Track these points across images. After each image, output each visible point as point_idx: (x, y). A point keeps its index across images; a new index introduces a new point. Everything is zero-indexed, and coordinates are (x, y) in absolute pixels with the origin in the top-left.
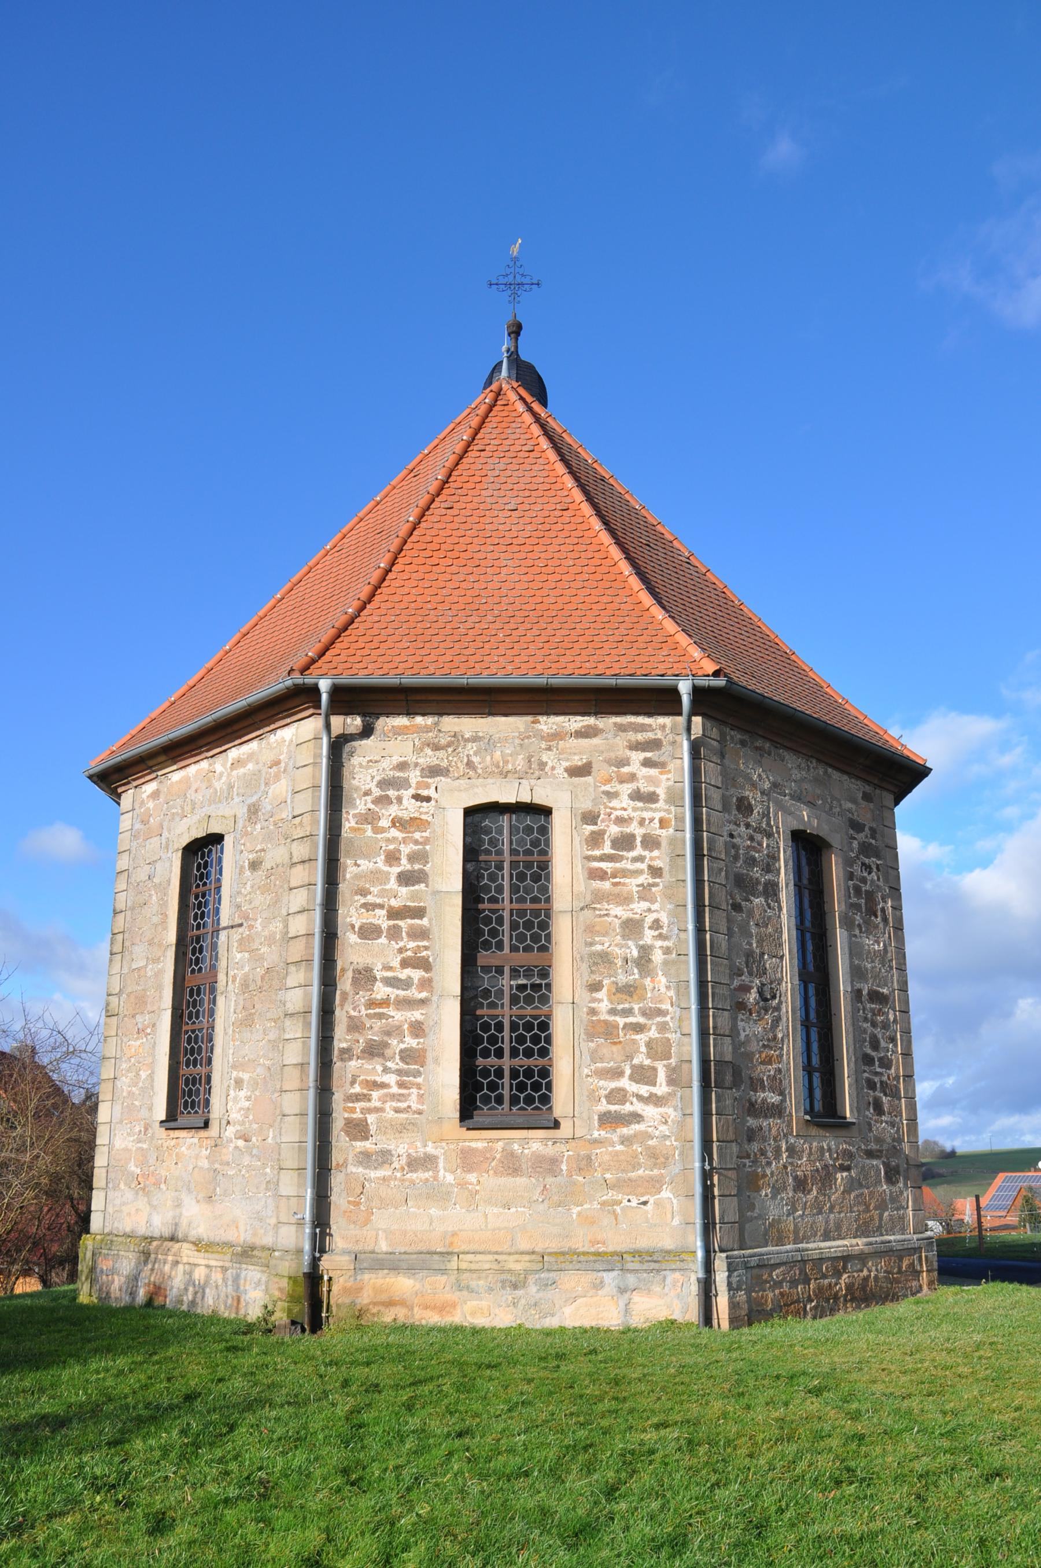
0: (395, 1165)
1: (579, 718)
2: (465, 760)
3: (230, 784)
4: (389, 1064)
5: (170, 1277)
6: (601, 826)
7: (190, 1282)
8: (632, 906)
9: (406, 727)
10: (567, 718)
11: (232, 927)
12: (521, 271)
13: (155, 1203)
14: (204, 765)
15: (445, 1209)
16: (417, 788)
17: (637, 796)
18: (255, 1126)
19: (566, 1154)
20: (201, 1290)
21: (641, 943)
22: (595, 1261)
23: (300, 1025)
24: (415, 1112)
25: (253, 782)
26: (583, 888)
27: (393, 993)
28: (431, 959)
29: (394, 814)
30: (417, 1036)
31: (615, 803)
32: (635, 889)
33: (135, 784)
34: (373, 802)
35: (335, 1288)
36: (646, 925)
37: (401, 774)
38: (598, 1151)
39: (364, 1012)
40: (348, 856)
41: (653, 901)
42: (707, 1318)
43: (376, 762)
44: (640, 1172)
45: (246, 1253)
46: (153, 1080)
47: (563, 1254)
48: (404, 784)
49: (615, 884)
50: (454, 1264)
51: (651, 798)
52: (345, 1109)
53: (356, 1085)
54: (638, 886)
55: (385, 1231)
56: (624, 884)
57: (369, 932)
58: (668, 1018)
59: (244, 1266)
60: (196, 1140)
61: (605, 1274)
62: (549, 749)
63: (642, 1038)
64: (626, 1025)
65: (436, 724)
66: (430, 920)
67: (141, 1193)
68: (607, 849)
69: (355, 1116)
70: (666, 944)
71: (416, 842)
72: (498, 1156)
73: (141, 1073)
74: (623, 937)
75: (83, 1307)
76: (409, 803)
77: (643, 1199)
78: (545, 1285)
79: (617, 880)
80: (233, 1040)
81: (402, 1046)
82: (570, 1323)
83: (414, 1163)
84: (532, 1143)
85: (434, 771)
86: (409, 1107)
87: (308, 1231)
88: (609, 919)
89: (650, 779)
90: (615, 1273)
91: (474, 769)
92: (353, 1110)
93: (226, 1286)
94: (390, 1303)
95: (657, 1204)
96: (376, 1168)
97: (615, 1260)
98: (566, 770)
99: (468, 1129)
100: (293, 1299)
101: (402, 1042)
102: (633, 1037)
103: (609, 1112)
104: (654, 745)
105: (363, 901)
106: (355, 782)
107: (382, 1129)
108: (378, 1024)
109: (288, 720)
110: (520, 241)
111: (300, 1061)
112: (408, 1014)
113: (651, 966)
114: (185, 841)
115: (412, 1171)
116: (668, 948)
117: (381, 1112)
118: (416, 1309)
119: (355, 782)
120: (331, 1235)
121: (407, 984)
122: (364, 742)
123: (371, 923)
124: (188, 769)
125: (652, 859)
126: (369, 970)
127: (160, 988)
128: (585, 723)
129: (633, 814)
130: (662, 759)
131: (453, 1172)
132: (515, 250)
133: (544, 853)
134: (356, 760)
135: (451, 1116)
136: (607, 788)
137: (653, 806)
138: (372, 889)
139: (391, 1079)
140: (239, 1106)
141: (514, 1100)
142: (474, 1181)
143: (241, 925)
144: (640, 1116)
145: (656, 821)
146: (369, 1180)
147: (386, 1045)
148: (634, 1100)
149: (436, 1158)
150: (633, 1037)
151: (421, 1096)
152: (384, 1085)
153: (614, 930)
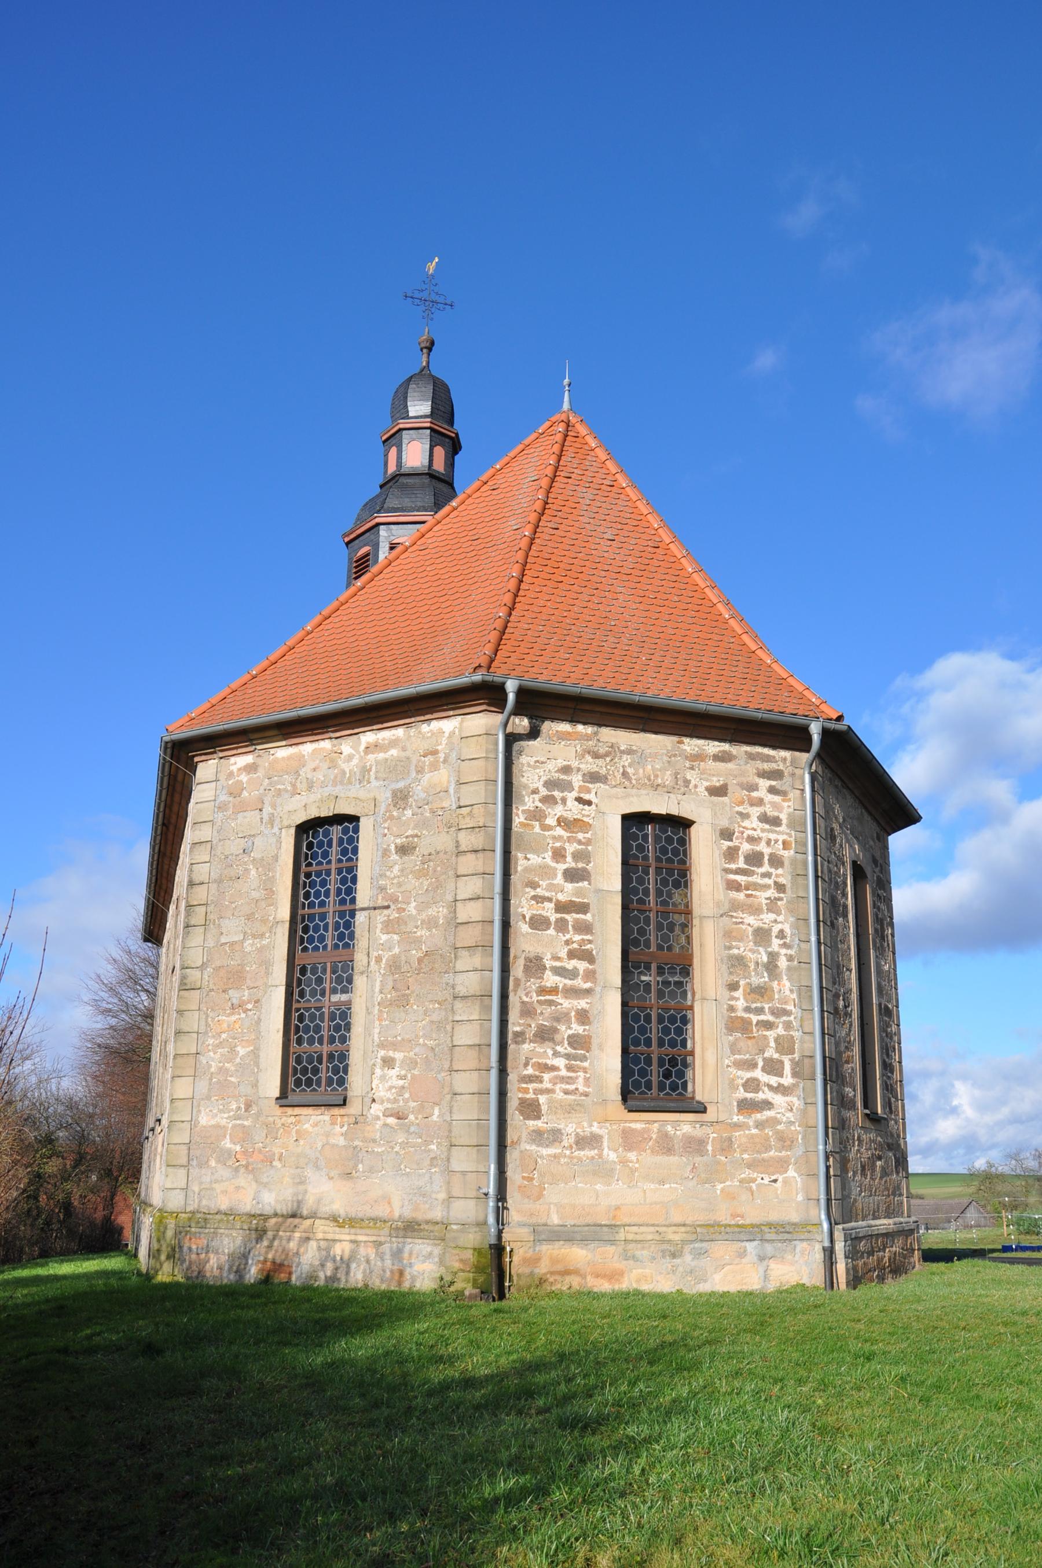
0: (565, 1143)
1: (716, 743)
2: (621, 770)
3: (364, 767)
4: (559, 1048)
5: (297, 1253)
6: (735, 843)
7: (327, 1256)
8: (762, 917)
9: (569, 733)
10: (707, 741)
11: (375, 909)
12: (436, 289)
13: (265, 1180)
14: (326, 745)
15: (609, 1185)
16: (579, 792)
17: (764, 818)
18: (412, 1104)
19: (712, 1136)
20: (346, 1263)
21: (770, 950)
22: (740, 1233)
23: (477, 1007)
24: (582, 1094)
25: (399, 768)
26: (722, 897)
27: (561, 982)
28: (594, 952)
29: (559, 814)
30: (583, 1023)
31: (746, 823)
32: (764, 902)
33: (221, 754)
34: (540, 801)
35: (515, 1258)
36: (774, 934)
37: (565, 777)
38: (737, 1134)
39: (535, 998)
40: (518, 849)
41: (779, 914)
42: (830, 1281)
43: (542, 763)
44: (772, 1153)
45: (410, 1228)
46: (257, 1057)
47: (712, 1226)
48: (567, 786)
49: (748, 896)
50: (621, 1236)
51: (775, 822)
52: (520, 1090)
53: (529, 1067)
54: (767, 899)
55: (556, 1205)
56: (755, 897)
57: (538, 923)
58: (792, 1018)
59: (409, 1240)
60: (327, 1118)
61: (747, 1244)
62: (692, 768)
63: (771, 1034)
64: (758, 1023)
65: (596, 734)
66: (593, 916)
67: (242, 1170)
68: (741, 864)
69: (528, 1096)
70: (789, 952)
71: (580, 842)
72: (654, 1136)
73: (239, 1049)
74: (755, 943)
75: (164, 1286)
76: (571, 803)
77: (773, 1178)
78: (699, 1254)
79: (749, 892)
80: (380, 1020)
81: (570, 1032)
82: (720, 1288)
83: (584, 1142)
84: (682, 1125)
85: (594, 777)
86: (577, 1089)
87: (491, 1204)
88: (744, 927)
89: (775, 805)
90: (756, 1243)
91: (629, 779)
92: (526, 1091)
93: (383, 1260)
94: (566, 1272)
95: (785, 1182)
96: (547, 1146)
97: (754, 1232)
98: (707, 789)
99: (629, 1111)
100: (479, 1269)
101: (570, 1028)
102: (765, 1033)
103: (746, 1099)
104: (776, 775)
105: (533, 893)
106: (524, 780)
107: (556, 1107)
108: (548, 1010)
109: (451, 713)
110: (437, 260)
111: (476, 1041)
112: (575, 1002)
113: (778, 971)
114: (301, 818)
115: (579, 1149)
116: (791, 956)
117: (550, 1094)
118: (589, 1278)
119: (524, 780)
120: (507, 1209)
121: (573, 974)
122: (531, 743)
123: (540, 915)
124: (301, 747)
125: (777, 876)
126: (539, 959)
127: (267, 965)
128: (722, 749)
129: (761, 835)
130: (783, 788)
131: (616, 1151)
132: (431, 267)
133: (683, 862)
134: (524, 759)
135: (614, 1098)
136: (740, 809)
137: (777, 829)
138: (541, 883)
139: (560, 1062)
140: (389, 1084)
141: (661, 1087)
142: (634, 1158)
143: (388, 907)
144: (770, 1103)
145: (780, 842)
146: (541, 1157)
147: (556, 1030)
148: (766, 1089)
149: (601, 1137)
150: (765, 1033)
151: (587, 1080)
152: (554, 1068)
153: (748, 937)
